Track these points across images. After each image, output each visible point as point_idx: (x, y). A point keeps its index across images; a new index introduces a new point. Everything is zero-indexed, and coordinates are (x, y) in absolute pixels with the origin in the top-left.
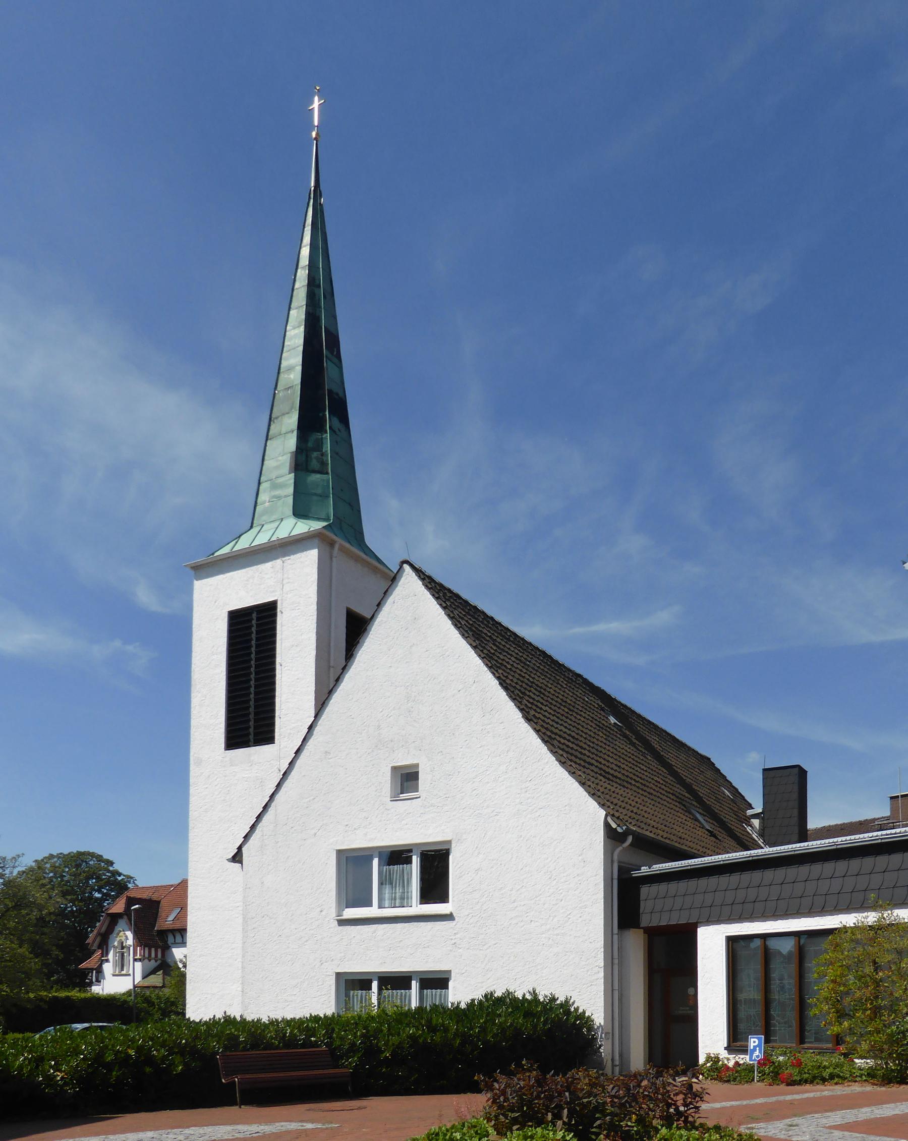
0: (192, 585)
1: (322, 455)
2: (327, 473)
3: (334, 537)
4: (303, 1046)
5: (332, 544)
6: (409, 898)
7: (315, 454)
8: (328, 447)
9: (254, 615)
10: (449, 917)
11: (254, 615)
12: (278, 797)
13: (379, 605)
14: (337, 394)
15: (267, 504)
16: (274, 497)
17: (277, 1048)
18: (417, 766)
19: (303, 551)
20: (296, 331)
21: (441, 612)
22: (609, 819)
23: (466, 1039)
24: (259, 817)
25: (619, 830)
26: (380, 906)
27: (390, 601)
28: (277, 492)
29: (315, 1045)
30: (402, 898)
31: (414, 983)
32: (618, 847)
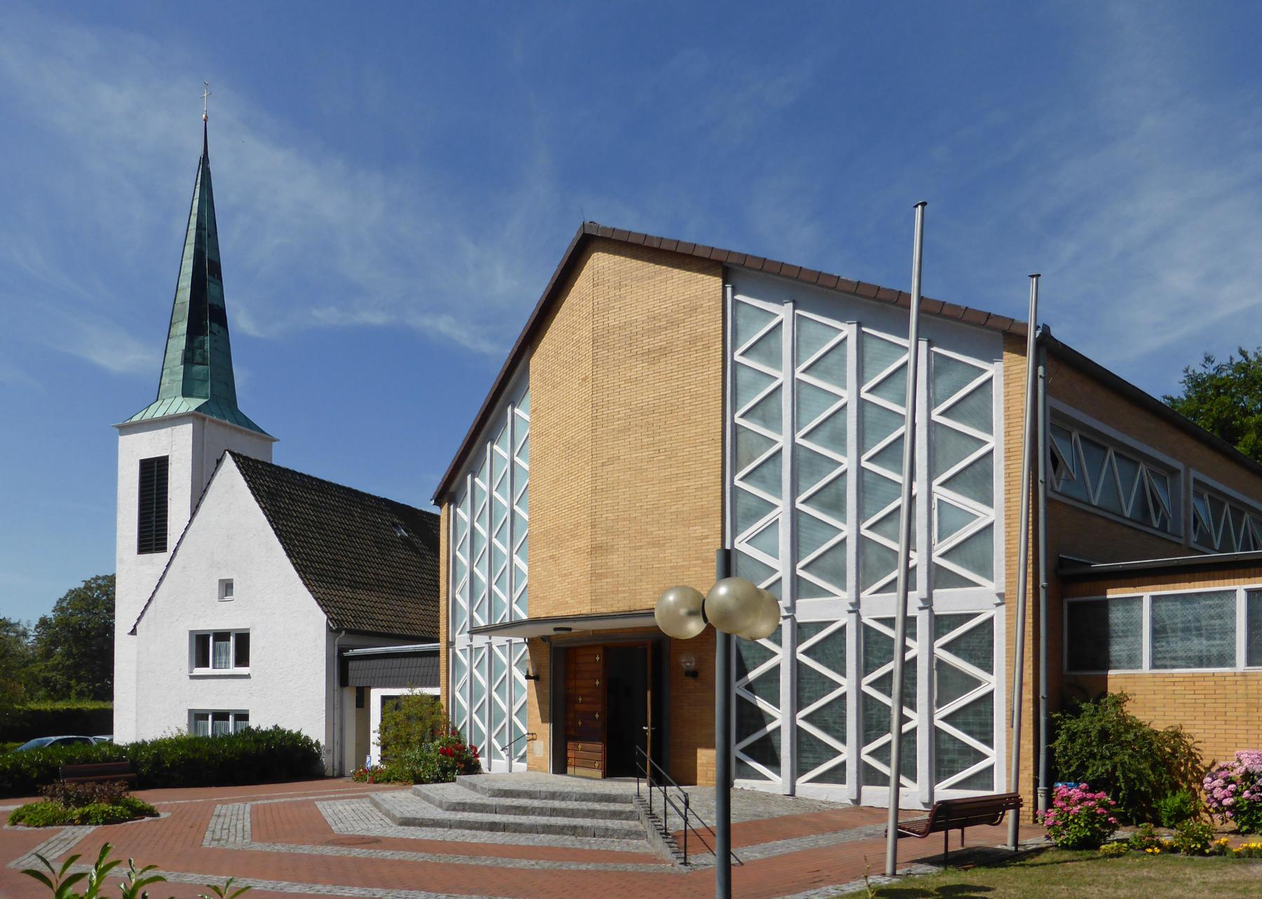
1: (204, 351)
2: (207, 365)
3: (205, 415)
4: (117, 761)
5: (204, 419)
7: (199, 351)
8: (207, 346)
9: (156, 464)
10: (248, 676)
11: (156, 464)
12: (157, 594)
13: (213, 475)
14: (218, 306)
15: (167, 385)
16: (171, 380)
17: (100, 762)
18: (232, 579)
19: (183, 424)
20: (188, 261)
21: (245, 484)
22: (329, 621)
24: (146, 607)
25: (334, 628)
26: (214, 668)
27: (219, 473)
28: (173, 378)
29: (124, 760)
30: (225, 663)
31: (231, 716)
32: (336, 637)
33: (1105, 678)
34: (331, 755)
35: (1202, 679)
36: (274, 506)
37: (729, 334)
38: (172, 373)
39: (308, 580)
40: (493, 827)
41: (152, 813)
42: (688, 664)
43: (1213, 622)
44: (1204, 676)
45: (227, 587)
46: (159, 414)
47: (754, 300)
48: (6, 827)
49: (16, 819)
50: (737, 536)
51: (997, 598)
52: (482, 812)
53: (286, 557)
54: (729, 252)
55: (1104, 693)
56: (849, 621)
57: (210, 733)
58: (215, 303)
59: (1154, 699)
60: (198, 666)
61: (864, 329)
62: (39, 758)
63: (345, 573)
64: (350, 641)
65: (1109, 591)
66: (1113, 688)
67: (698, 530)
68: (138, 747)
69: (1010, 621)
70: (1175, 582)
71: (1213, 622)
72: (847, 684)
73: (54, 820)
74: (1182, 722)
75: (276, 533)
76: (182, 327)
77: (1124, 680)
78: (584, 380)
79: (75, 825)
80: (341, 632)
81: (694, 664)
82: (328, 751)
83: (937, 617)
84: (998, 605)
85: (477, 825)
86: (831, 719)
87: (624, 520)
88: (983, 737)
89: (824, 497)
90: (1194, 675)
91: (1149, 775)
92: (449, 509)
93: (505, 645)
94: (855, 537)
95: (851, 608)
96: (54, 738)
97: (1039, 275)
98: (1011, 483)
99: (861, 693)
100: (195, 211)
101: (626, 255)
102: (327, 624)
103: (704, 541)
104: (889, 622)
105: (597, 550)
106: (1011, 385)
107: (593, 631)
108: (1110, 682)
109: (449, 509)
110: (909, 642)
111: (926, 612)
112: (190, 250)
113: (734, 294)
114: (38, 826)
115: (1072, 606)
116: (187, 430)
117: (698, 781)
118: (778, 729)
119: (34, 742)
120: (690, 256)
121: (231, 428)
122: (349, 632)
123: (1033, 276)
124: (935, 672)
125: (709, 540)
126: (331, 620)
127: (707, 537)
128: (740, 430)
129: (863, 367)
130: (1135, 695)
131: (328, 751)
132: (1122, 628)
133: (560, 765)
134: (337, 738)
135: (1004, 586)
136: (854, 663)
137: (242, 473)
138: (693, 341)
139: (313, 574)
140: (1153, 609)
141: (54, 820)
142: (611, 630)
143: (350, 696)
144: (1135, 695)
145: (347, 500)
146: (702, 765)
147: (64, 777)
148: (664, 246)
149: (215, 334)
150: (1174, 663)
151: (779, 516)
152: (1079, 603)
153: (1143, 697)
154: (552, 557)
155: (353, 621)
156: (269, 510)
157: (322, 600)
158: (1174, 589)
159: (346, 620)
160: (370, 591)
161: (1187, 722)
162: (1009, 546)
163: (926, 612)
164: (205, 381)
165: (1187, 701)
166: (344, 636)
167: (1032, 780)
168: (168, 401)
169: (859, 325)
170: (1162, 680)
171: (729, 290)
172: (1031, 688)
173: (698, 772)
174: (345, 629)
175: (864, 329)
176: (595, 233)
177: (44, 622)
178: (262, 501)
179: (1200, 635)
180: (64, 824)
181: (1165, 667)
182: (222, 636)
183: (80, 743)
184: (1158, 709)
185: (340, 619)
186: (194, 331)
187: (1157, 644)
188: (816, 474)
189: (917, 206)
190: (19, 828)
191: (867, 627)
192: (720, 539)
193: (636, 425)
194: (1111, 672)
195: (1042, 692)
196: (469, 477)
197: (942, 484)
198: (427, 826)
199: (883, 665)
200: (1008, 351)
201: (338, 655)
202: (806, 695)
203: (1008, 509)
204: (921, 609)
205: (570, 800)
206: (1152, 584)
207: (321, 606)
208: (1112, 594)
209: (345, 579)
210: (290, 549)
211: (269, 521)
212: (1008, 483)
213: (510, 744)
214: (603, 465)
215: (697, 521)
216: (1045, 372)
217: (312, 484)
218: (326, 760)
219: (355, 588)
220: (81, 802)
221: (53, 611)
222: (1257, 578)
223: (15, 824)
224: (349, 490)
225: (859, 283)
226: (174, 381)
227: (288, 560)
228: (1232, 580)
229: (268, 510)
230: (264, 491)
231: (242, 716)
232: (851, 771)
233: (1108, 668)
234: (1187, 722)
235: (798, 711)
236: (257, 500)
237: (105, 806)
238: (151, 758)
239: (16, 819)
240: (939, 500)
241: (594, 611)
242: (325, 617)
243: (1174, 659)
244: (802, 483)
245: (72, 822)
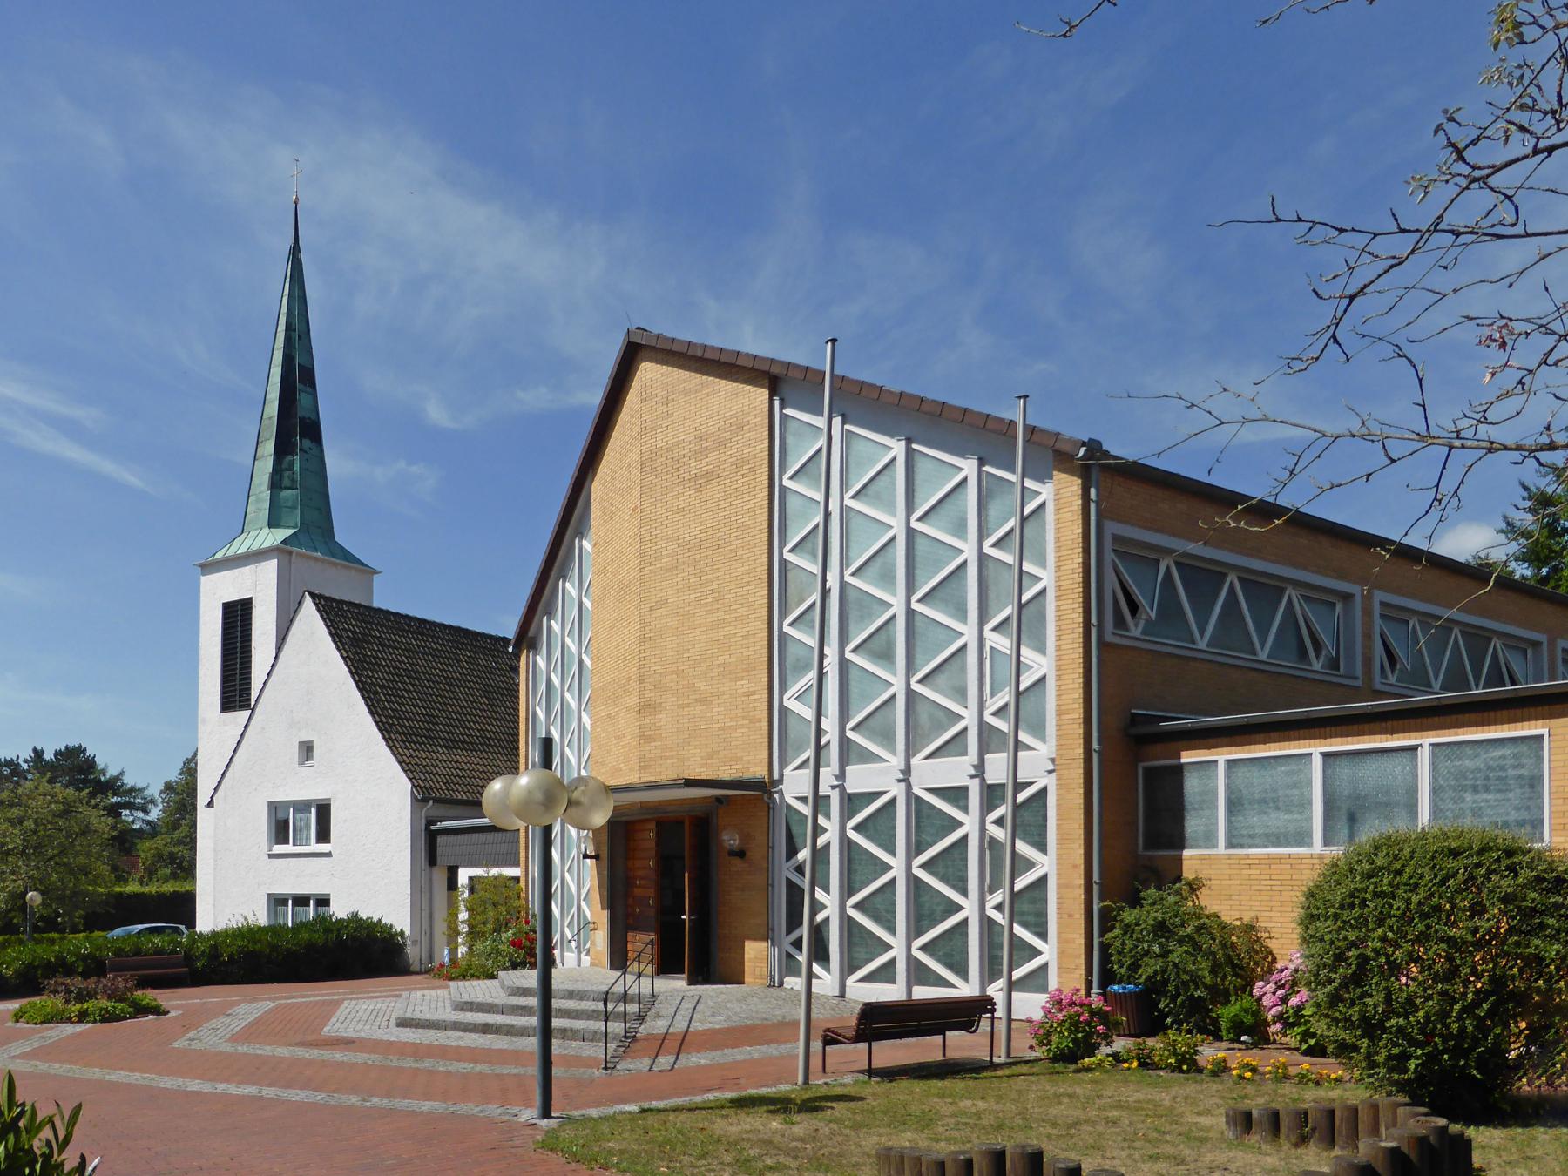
0: (199, 579)
6: (308, 838)
7: (287, 474)
8: (297, 467)
10: (329, 855)
11: (239, 607)
12: (234, 759)
14: (309, 418)
23: (274, 948)
24: (223, 775)
26: (294, 845)
29: (177, 952)
33: (1180, 860)
34: (418, 947)
35: (1278, 861)
36: (358, 654)
37: (775, 458)
38: (258, 501)
39: (392, 740)
40: (486, 1029)
41: (157, 1011)
42: (732, 842)
43: (1289, 792)
44: (1280, 858)
45: (307, 750)
46: (242, 550)
47: (803, 414)
48: (10, 1024)
49: (18, 1017)
50: (786, 691)
51: (1050, 763)
52: (488, 1012)
53: (368, 715)
54: (772, 360)
55: (1179, 878)
56: (897, 790)
59: (1230, 885)
60: (278, 843)
61: (914, 446)
62: (86, 949)
63: (441, 731)
64: (440, 811)
65: (1183, 753)
66: (1188, 873)
67: (744, 685)
68: (215, 934)
69: (1061, 792)
70: (1250, 744)
71: (1289, 792)
72: (897, 864)
73: (52, 1018)
74: (1258, 914)
75: (358, 687)
76: (269, 447)
77: (1199, 862)
78: (634, 510)
79: (73, 1022)
81: (737, 842)
82: (414, 942)
83: (990, 786)
84: (1050, 772)
85: (470, 1027)
86: (880, 907)
87: (672, 673)
88: (1038, 930)
89: (873, 645)
90: (1269, 857)
91: (1205, 977)
92: (528, 657)
93: (966, 788)
94: (904, 692)
95: (901, 777)
96: (140, 927)
97: (1027, 396)
98: (1063, 627)
99: (912, 878)
100: (284, 309)
101: (673, 366)
102: (412, 792)
103: (751, 697)
104: (803, 800)
105: (646, 708)
106: (1061, 511)
107: (641, 803)
108: (1185, 863)
109: (528, 657)
110: (821, 821)
111: (977, 780)
112: (278, 356)
113: (782, 408)
114: (36, 1024)
115: (1147, 771)
116: (270, 567)
117: (746, 980)
118: (827, 920)
119: (119, 931)
120: (734, 366)
121: (323, 561)
122: (437, 801)
123: (1020, 397)
124: (987, 852)
125: (756, 697)
126: (416, 787)
127: (754, 693)
128: (789, 567)
129: (913, 491)
130: (1210, 880)
131: (414, 942)
132: (1198, 798)
133: (619, 958)
134: (425, 926)
135: (1054, 749)
136: (904, 841)
137: (322, 617)
138: (739, 464)
139: (400, 734)
140: (1228, 775)
141: (52, 1018)
142: (659, 801)
143: (440, 877)
144: (1210, 880)
145: (454, 641)
146: (750, 960)
147: (113, 970)
148: (708, 355)
149: (306, 452)
150: (1249, 841)
152: (1156, 768)
153: (1218, 882)
154: (609, 716)
155: (444, 788)
156: (351, 660)
157: (407, 764)
158: (1249, 752)
159: (436, 788)
160: (471, 751)
161: (1263, 914)
162: (1060, 702)
163: (977, 780)
164: (293, 508)
165: (1264, 888)
167: (1083, 981)
168: (253, 533)
169: (909, 441)
170: (1237, 862)
171: (777, 403)
172: (1082, 872)
173: (746, 968)
174: (433, 798)
175: (914, 446)
176: (639, 341)
177: (168, 787)
178: (344, 649)
179: (1278, 808)
180: (61, 1021)
181: (1242, 846)
182: (302, 806)
183: (170, 931)
184: (1233, 897)
185: (428, 786)
186: (283, 449)
187: (1233, 819)
188: (868, 616)
189: (827, 342)
190: (19, 1025)
191: (918, 798)
193: (684, 563)
194: (1186, 853)
195: (1096, 877)
196: (545, 619)
197: (995, 629)
198: (423, 1027)
199: (935, 843)
200: (1059, 471)
201: (426, 828)
202: (858, 878)
203: (1059, 658)
204: (972, 777)
205: (588, 1000)
206: (1227, 746)
207: (405, 771)
208: (1187, 757)
209: (440, 737)
210: (373, 705)
211: (351, 672)
212: (1059, 628)
213: (579, 932)
214: (651, 609)
215: (744, 674)
216: (1098, 495)
217: (409, 625)
218: (412, 952)
219: (451, 748)
220: (81, 998)
221: (180, 774)
222: (1333, 739)
223: (17, 1021)
224: (458, 630)
225: (901, 393)
226: (261, 510)
227: (370, 718)
228: (1307, 741)
229: (350, 659)
230: (348, 637)
231: (323, 901)
232: (901, 967)
233: (1183, 847)
234: (1263, 914)
235: (848, 898)
236: (338, 648)
237: (105, 1003)
238: (207, 951)
239: (18, 1017)
240: (991, 648)
241: (643, 779)
242: (410, 785)
243: (1251, 836)
244: (852, 628)
245: (69, 1020)
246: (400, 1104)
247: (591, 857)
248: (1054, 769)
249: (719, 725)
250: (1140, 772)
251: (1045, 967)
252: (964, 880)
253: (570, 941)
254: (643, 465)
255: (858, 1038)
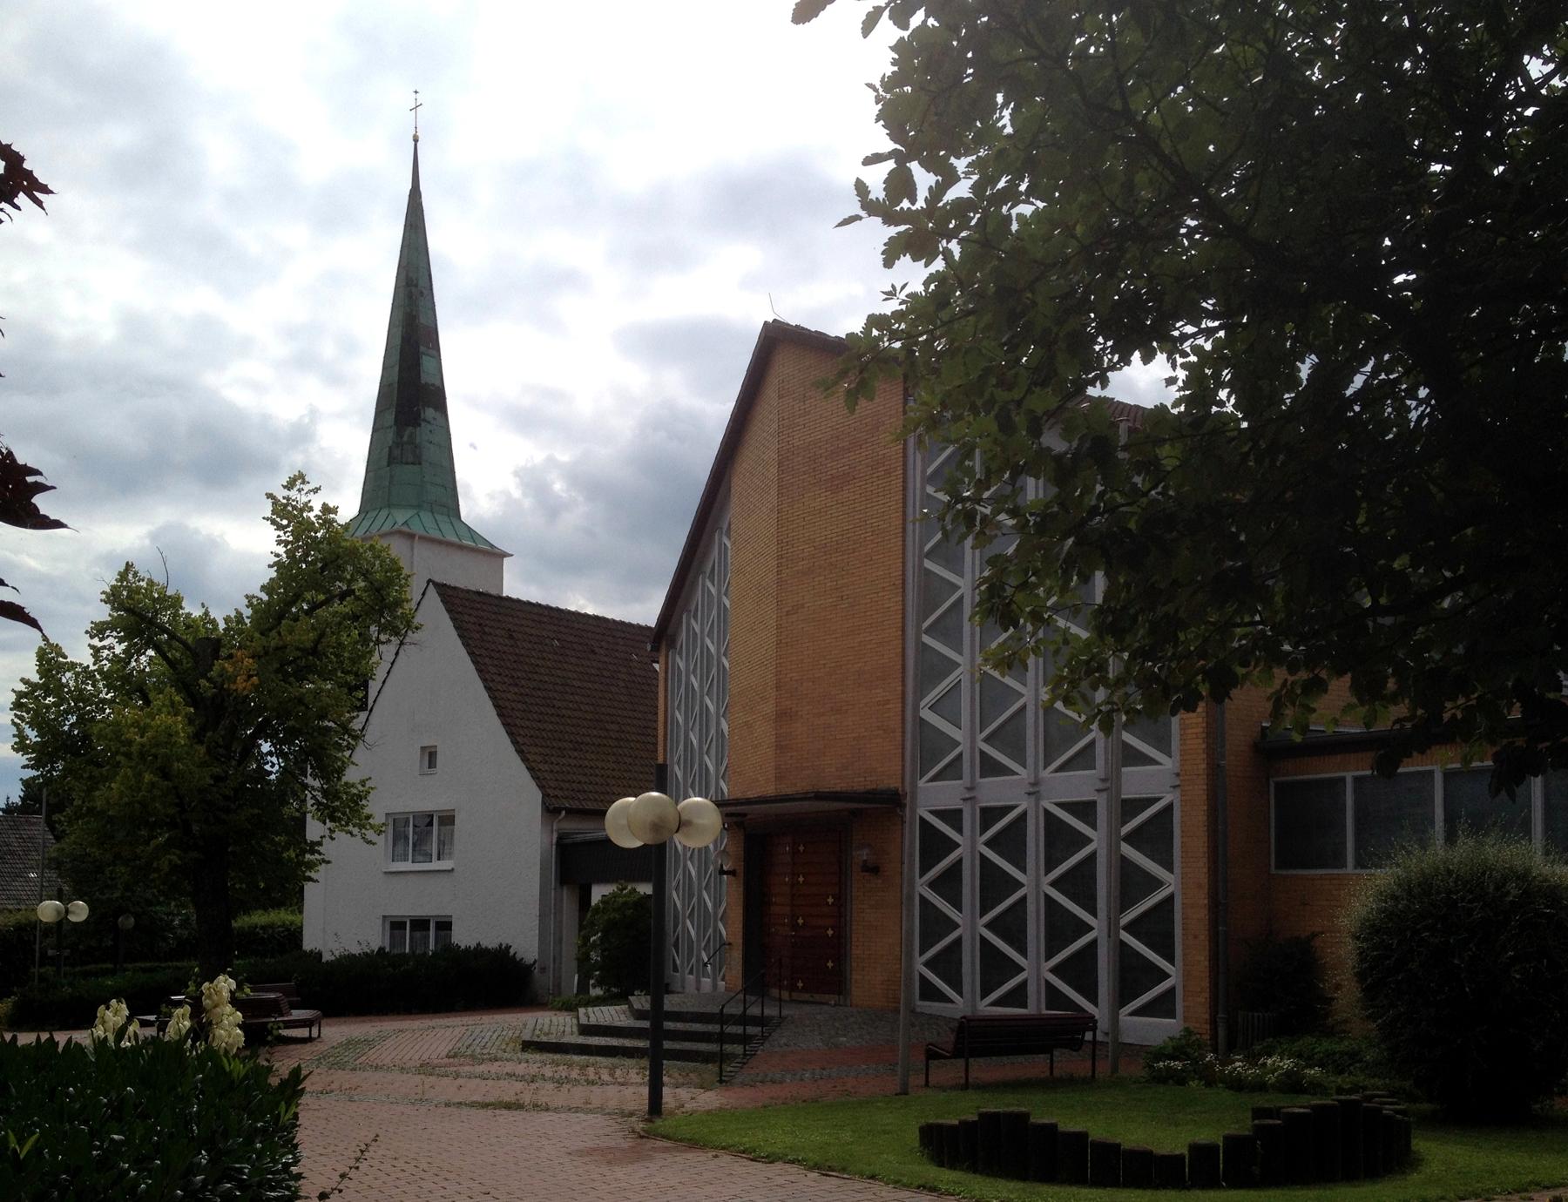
45: (431, 756)
57: (407, 951)
58: (430, 383)
80: (560, 813)
109: (667, 656)
115: (1280, 787)
135: (1178, 765)
151: (961, 677)
166: (565, 816)
174: (565, 809)
192: (900, 705)
196: (684, 616)
231: (445, 926)
246: (552, 931)
247: (727, 873)
248: (1181, 780)
249: (854, 735)
250: (1272, 784)
251: (1172, 991)
252: (1093, 898)
253: (705, 965)
254: (780, 464)
255: (957, 1053)
